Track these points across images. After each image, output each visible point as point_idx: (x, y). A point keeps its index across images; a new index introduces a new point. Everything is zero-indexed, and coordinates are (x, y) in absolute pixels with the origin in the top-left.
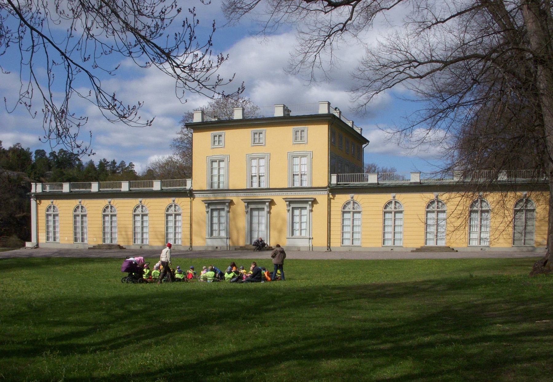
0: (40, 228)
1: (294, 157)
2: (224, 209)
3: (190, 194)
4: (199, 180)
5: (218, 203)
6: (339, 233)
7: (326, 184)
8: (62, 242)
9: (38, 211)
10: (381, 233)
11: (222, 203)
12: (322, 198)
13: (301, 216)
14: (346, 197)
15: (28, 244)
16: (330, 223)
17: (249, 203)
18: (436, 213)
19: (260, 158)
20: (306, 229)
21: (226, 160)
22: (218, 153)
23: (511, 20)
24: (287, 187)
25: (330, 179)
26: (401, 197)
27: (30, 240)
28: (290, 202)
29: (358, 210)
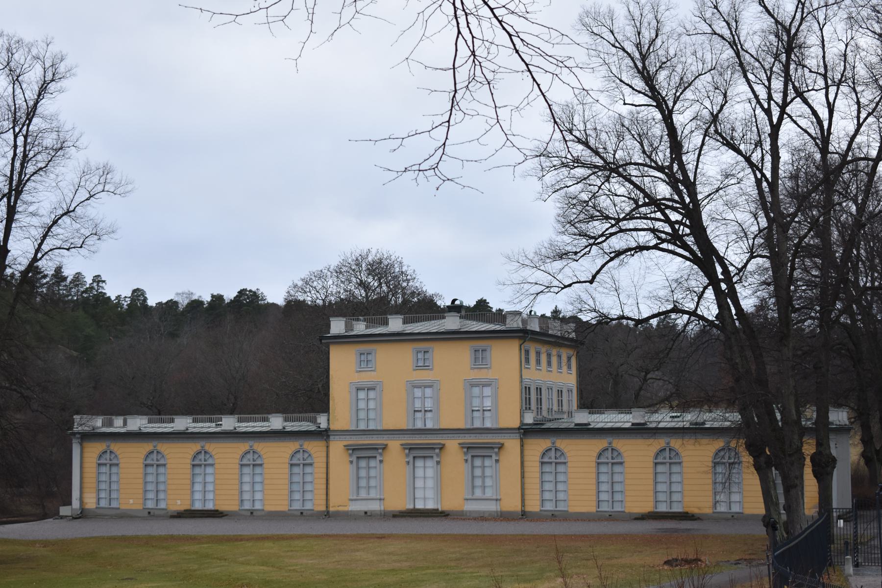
0: (86, 485)
1: (473, 385)
2: (432, 457)
3: (324, 435)
4: (341, 412)
5: (366, 449)
6: (538, 492)
7: (516, 424)
8: (123, 507)
9: (85, 461)
10: (594, 492)
11: (489, 447)
12: (512, 444)
13: (483, 467)
14: (544, 443)
15: (64, 511)
16: (327, 494)
17: (468, 448)
18: (668, 465)
19: (484, 386)
20: (376, 487)
21: (378, 388)
22: (367, 378)
23: (792, 288)
24: (405, 428)
25: (522, 417)
26: (563, 444)
27: (69, 503)
28: (411, 448)
29: (562, 460)
